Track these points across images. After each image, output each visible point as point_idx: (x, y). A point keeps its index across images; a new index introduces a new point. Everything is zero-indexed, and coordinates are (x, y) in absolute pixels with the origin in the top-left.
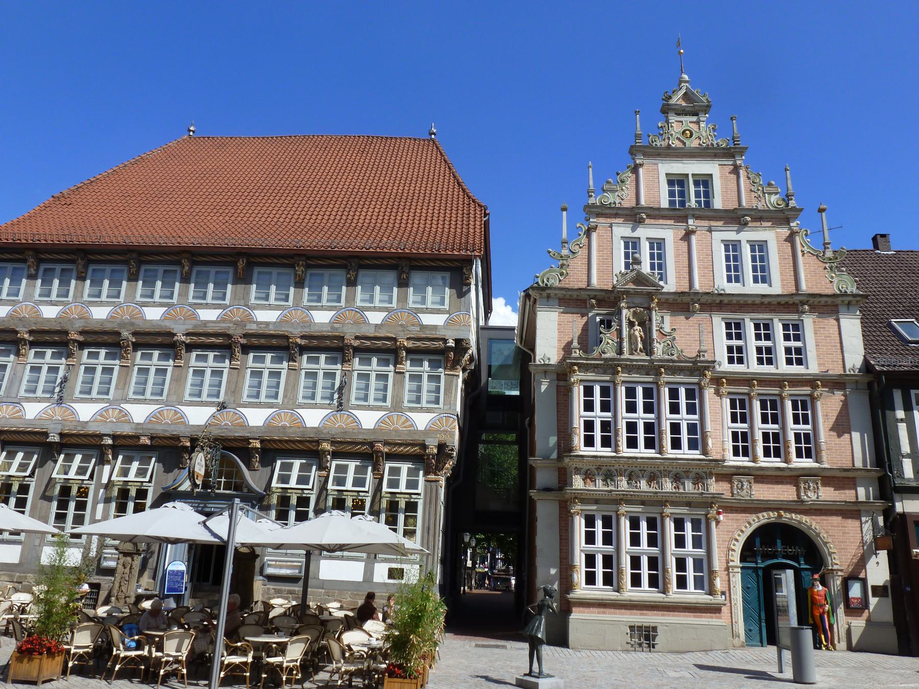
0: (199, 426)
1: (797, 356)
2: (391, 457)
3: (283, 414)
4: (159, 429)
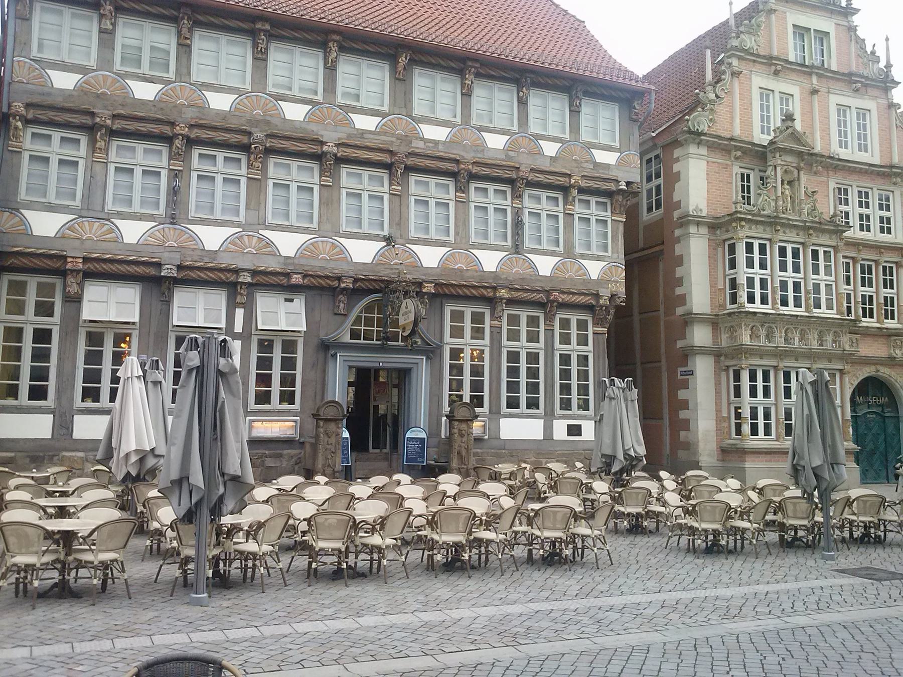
1: (886, 226)
2: (511, 302)
4: (315, 265)
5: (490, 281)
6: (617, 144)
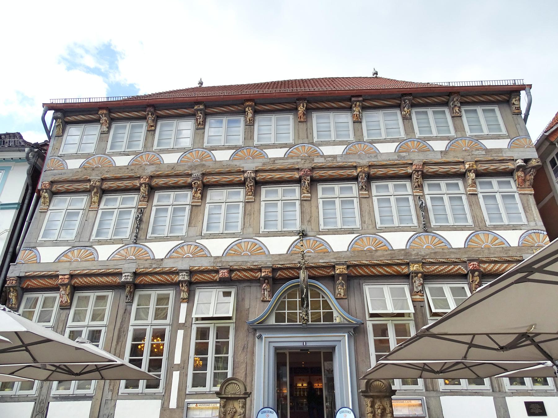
4: (234, 261)
5: (402, 258)
6: (504, 132)
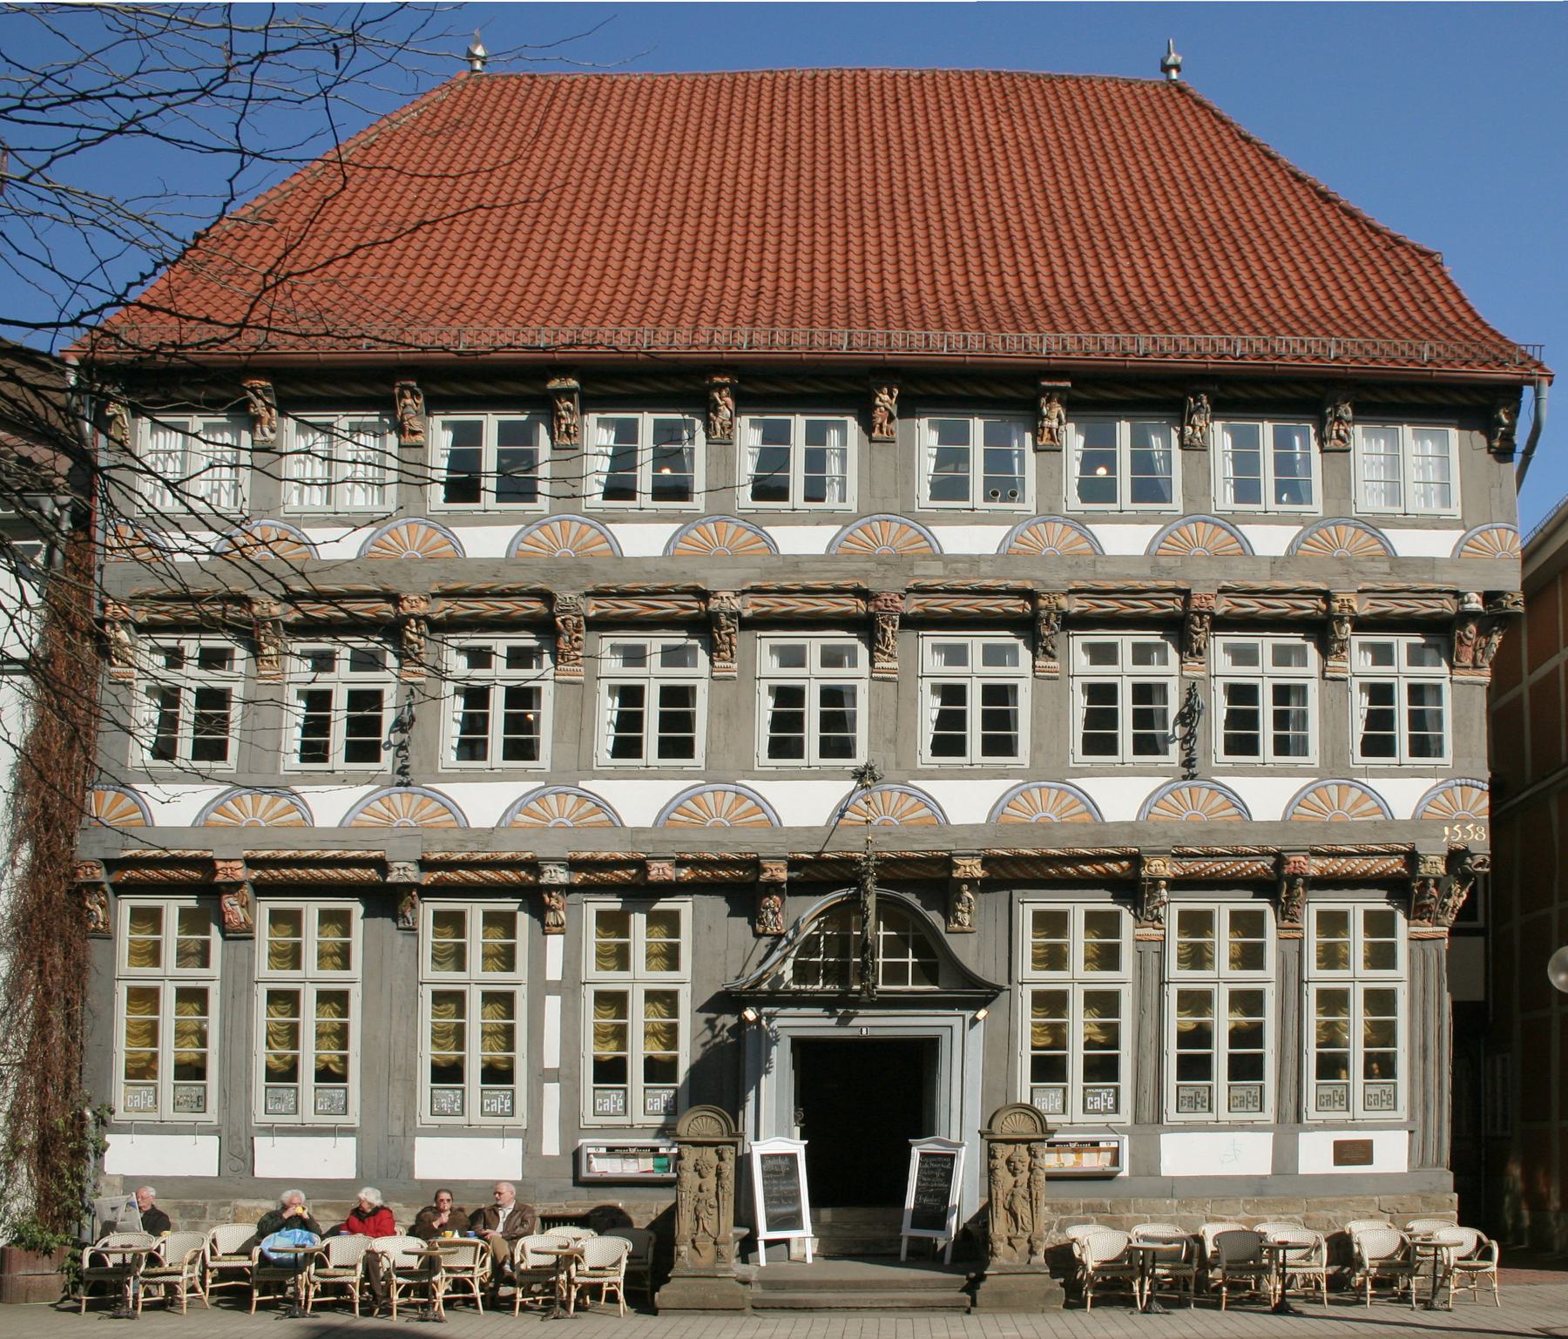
0: (809, 829)
3: (1036, 793)
